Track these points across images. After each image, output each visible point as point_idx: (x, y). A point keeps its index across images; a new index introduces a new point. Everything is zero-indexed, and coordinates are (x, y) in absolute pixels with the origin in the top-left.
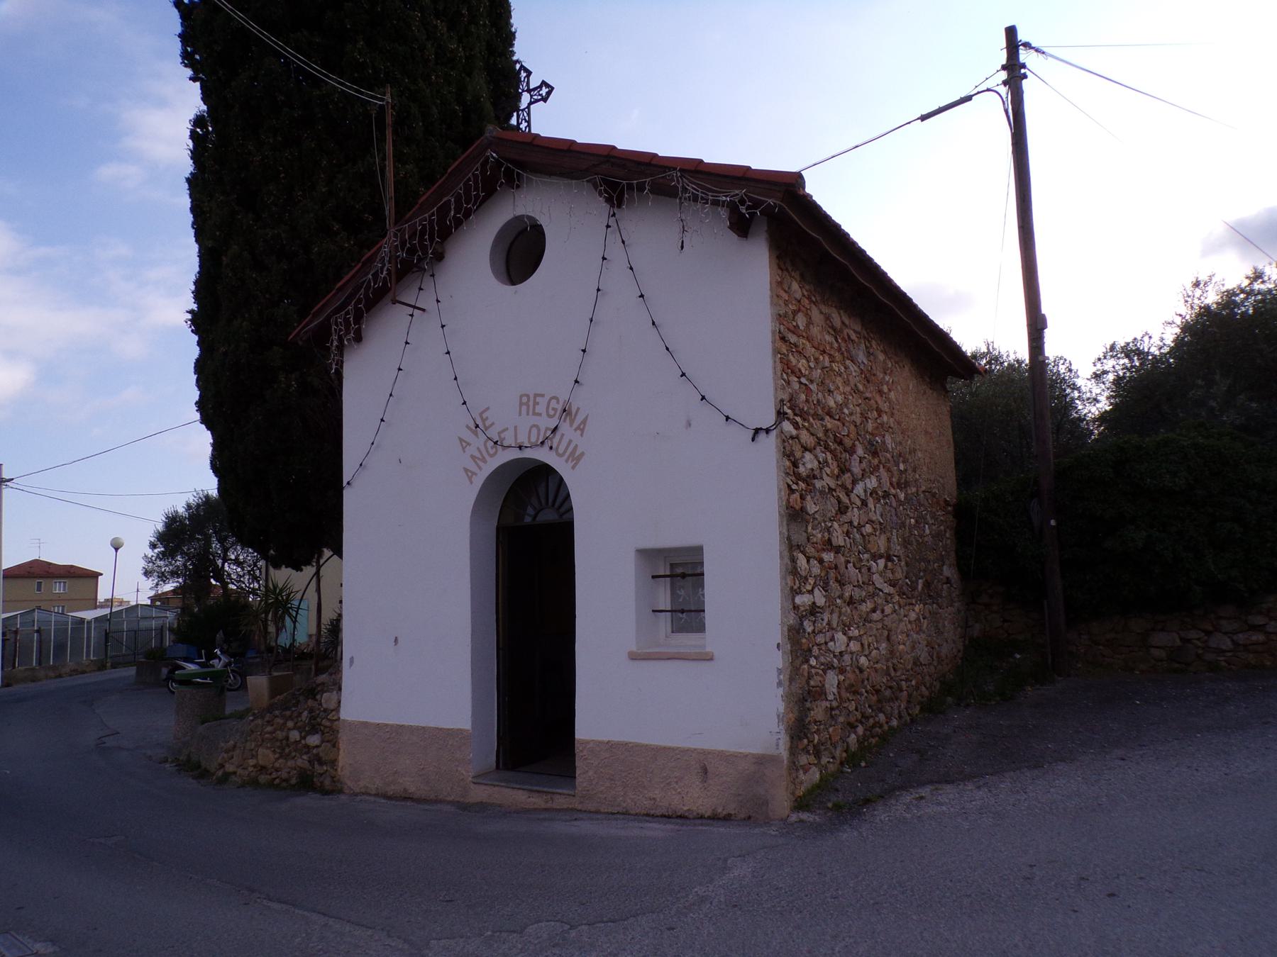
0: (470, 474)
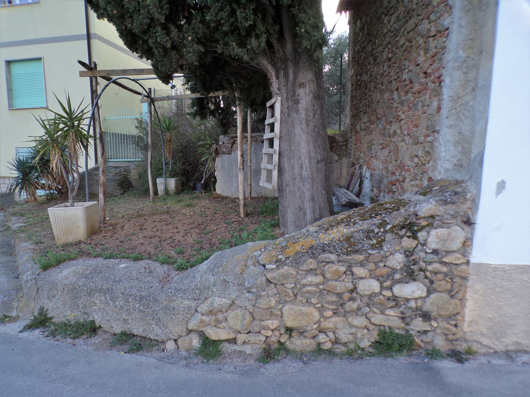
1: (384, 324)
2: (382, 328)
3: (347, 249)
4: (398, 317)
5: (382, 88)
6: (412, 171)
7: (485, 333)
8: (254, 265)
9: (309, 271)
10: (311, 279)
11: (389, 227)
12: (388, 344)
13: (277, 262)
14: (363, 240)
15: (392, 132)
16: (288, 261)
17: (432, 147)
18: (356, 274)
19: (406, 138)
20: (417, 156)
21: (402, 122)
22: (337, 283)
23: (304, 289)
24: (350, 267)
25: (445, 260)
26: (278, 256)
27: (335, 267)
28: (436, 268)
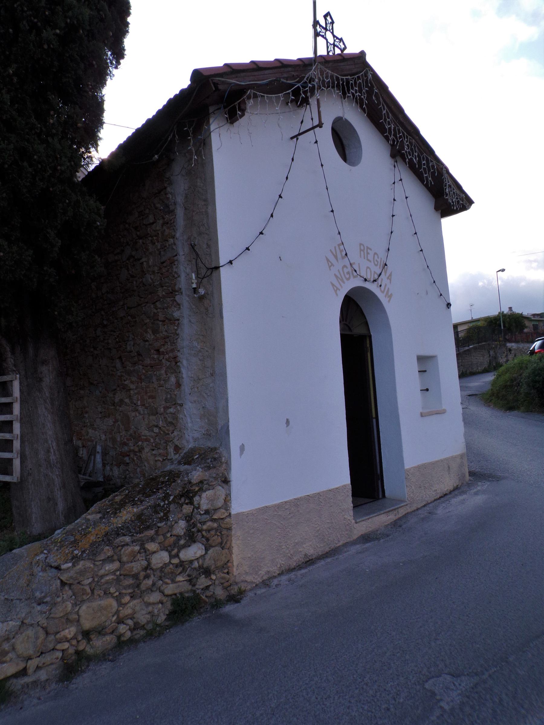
0: (336, 290)
1: (176, 592)
2: (174, 597)
3: (139, 528)
4: (186, 580)
5: (96, 352)
6: (152, 440)
7: (248, 571)
8: (44, 570)
10: (110, 567)
11: (172, 498)
12: (183, 609)
13: (72, 559)
14: (152, 516)
15: (117, 400)
16: (85, 555)
17: (176, 418)
18: (149, 550)
19: (140, 409)
20: (157, 426)
21: (132, 392)
23: (103, 581)
24: (142, 546)
25: (215, 517)
27: (129, 549)
28: (209, 526)
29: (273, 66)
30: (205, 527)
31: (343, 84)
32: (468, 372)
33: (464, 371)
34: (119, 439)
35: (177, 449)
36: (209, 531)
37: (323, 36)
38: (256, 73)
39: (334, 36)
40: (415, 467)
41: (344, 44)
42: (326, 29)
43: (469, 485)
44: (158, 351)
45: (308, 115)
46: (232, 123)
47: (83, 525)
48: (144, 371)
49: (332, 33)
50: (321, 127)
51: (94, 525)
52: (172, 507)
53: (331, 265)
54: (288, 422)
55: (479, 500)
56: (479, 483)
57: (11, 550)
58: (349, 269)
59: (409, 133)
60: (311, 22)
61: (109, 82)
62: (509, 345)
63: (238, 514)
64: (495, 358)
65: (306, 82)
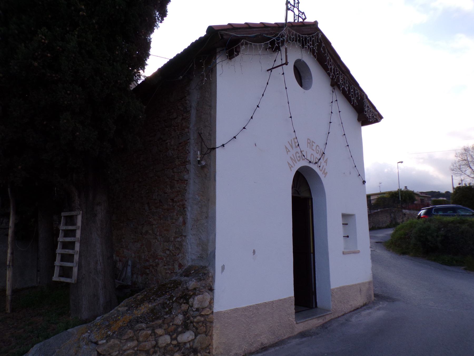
0: (291, 167)
6: (165, 259)
8: (87, 344)
9: (127, 340)
10: (130, 344)
11: (175, 299)
13: (106, 337)
15: (144, 231)
16: (115, 335)
18: (157, 334)
19: (158, 237)
20: (168, 250)
21: (154, 226)
22: (146, 343)
23: (125, 353)
25: (203, 313)
26: (107, 333)
27: (145, 332)
29: (259, 26)
30: (195, 320)
31: (302, 40)
32: (376, 226)
33: (374, 226)
34: (143, 257)
35: (180, 266)
36: (198, 323)
37: (292, 10)
38: (248, 30)
39: (299, 11)
40: (338, 288)
41: (305, 16)
42: (294, 6)
43: (374, 303)
44: (172, 200)
45: (279, 57)
46: (230, 59)
47: (115, 314)
48: (163, 213)
49: (298, 9)
50: (287, 65)
51: (123, 314)
52: (175, 304)
53: (288, 151)
54: (254, 252)
55: (380, 313)
56: (381, 303)
57: (66, 329)
58: (300, 154)
59: (343, 72)
60: (285, 2)
61: (156, 30)
62: (404, 211)
63: (218, 313)
64: (395, 219)
65: (279, 37)
